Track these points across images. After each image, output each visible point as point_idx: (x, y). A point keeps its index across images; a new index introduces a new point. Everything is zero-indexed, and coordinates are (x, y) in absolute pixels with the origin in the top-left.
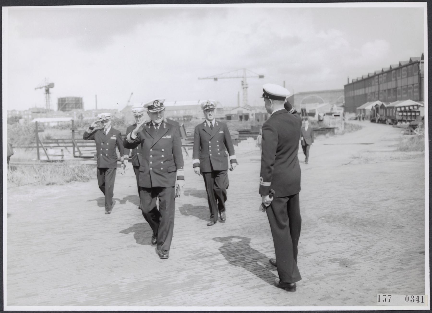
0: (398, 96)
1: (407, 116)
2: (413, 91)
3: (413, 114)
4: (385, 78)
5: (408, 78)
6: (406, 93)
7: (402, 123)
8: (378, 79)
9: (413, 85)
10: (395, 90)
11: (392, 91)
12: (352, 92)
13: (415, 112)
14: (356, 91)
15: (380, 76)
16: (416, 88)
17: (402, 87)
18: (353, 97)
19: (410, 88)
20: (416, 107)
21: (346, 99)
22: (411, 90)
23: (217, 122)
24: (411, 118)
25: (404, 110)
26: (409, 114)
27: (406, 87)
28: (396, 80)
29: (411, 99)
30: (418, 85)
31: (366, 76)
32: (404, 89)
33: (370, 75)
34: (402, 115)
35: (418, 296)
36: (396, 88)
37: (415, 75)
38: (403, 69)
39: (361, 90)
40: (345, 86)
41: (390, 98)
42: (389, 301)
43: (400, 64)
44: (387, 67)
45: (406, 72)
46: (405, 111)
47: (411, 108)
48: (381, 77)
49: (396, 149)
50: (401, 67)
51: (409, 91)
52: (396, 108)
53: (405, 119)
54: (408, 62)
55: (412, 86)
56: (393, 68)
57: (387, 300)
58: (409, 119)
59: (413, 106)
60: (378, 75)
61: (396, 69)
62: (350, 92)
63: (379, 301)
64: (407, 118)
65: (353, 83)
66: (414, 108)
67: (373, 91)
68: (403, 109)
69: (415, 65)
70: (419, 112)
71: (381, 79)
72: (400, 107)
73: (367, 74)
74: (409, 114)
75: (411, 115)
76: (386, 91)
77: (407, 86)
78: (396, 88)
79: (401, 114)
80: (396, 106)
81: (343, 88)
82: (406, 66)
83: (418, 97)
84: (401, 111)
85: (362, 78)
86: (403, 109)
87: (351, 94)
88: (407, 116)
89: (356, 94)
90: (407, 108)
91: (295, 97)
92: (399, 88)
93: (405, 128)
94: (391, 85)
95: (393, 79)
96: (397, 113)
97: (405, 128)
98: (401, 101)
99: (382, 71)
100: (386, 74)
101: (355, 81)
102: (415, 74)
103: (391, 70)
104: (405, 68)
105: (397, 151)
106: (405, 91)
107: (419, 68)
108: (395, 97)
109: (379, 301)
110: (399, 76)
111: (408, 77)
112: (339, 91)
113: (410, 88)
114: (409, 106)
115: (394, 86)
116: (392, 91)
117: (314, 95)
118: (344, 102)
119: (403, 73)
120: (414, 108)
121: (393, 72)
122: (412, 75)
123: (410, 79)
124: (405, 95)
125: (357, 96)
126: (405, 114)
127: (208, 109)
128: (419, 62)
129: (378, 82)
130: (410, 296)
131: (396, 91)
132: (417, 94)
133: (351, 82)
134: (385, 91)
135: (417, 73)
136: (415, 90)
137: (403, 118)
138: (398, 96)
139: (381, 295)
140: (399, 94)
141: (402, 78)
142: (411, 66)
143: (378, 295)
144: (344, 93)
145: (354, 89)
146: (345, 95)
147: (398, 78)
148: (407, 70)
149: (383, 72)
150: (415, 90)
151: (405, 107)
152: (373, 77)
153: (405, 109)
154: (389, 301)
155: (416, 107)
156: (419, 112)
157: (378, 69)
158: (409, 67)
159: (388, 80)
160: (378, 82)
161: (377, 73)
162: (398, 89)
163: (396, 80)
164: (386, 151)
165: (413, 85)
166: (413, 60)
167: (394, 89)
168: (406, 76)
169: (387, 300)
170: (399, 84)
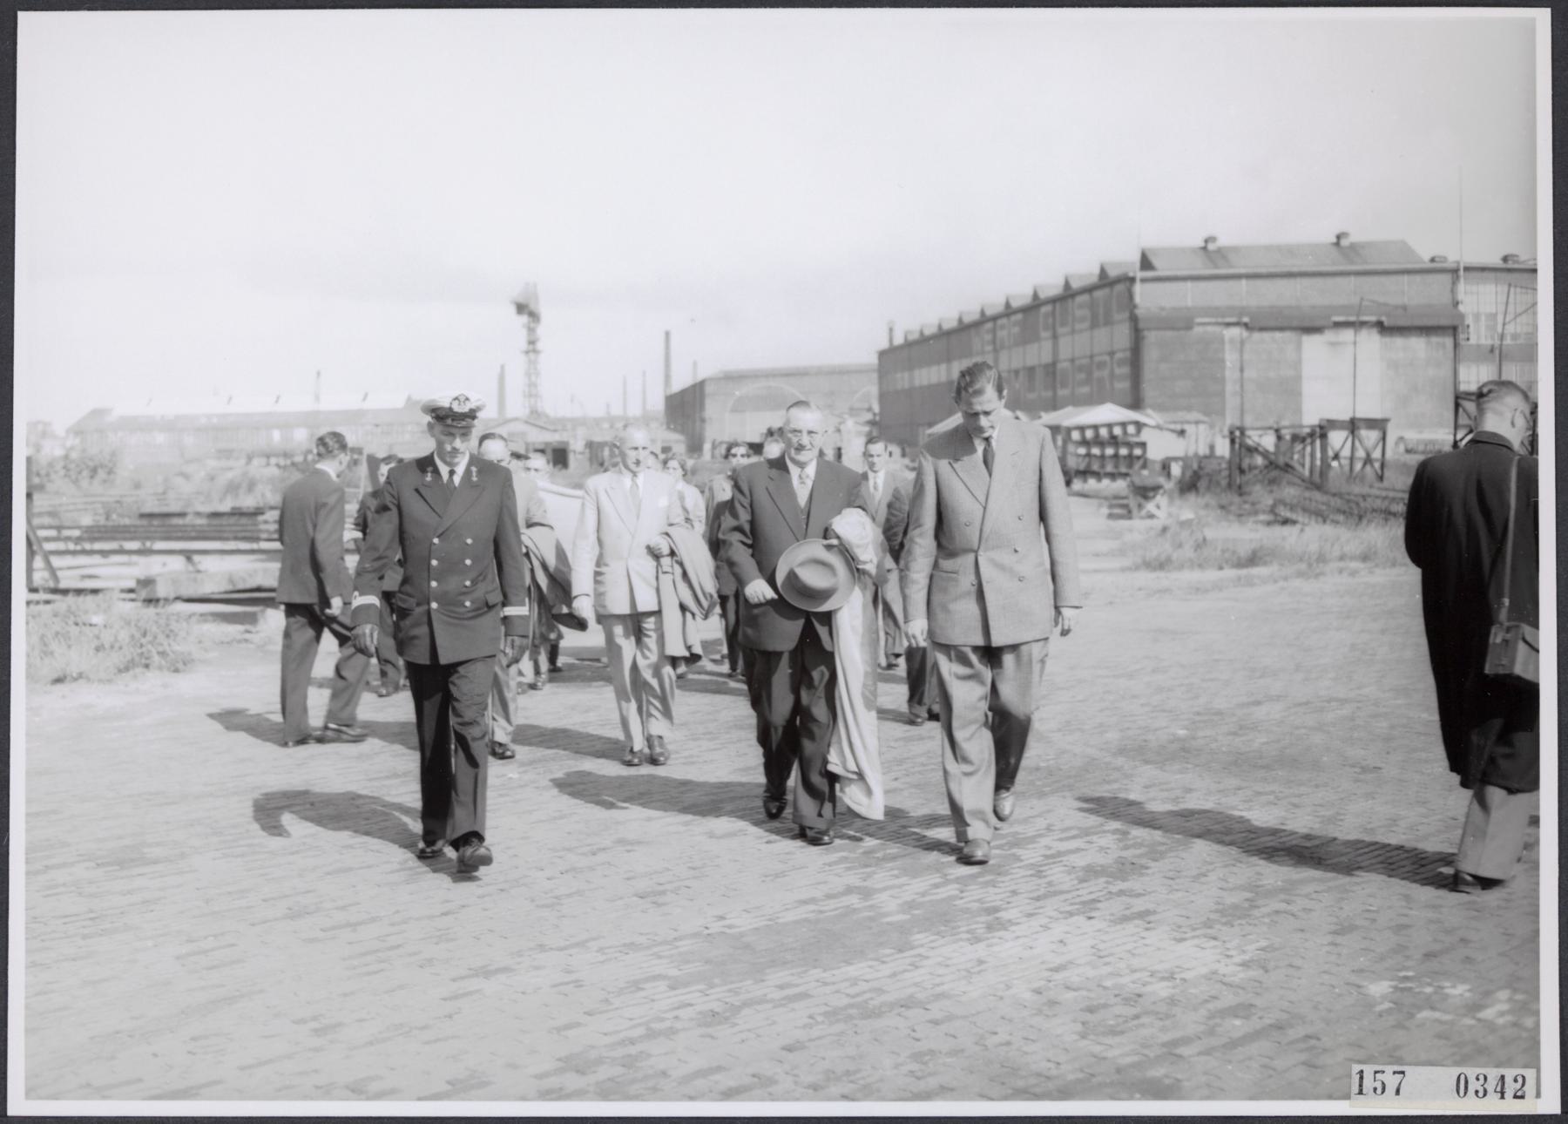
0: (1062, 392)
1: (1103, 457)
2: (1112, 376)
3: (1124, 451)
4: (1016, 330)
5: (1097, 332)
6: (1088, 381)
7: (1085, 481)
8: (994, 331)
9: (1111, 354)
10: (1051, 369)
11: (1039, 374)
12: (906, 375)
13: (1130, 445)
14: (917, 373)
15: (1000, 322)
16: (1121, 363)
17: (1072, 360)
18: (910, 393)
19: (1101, 365)
20: (1131, 429)
21: (882, 397)
22: (1105, 373)
23: (474, 469)
24: (1116, 466)
25: (1095, 438)
26: (1110, 451)
27: (1085, 361)
28: (1055, 337)
29: (1114, 402)
30: (1128, 354)
31: (951, 324)
32: (1080, 369)
33: (967, 319)
34: (1088, 455)
35: (1503, 1077)
36: (1054, 364)
37: (1081, 331)
38: (1080, 299)
39: (934, 369)
40: (882, 354)
41: (1032, 396)
42: (1398, 1092)
43: (1067, 285)
44: (1021, 293)
45: (1086, 312)
46: (1098, 441)
47: (1117, 431)
48: (1002, 327)
49: (1127, 562)
50: (1068, 294)
51: (1096, 374)
52: (1069, 430)
53: (1095, 467)
54: (1094, 279)
55: (1107, 358)
56: (1042, 295)
57: (1391, 1089)
58: (1109, 468)
59: (1124, 425)
60: (995, 318)
61: (1054, 301)
62: (899, 375)
63: (1361, 1093)
64: (1103, 466)
65: (909, 344)
66: (1125, 432)
67: (1031, 361)
68: (1089, 434)
69: (1120, 288)
70: (1143, 445)
71: (1002, 334)
72: (1082, 429)
73: (936, 322)
74: (1110, 451)
75: (1116, 456)
76: (1021, 374)
77: (1091, 357)
78: (1054, 364)
79: (1082, 451)
80: (1067, 423)
81: (873, 360)
82: (1089, 290)
83: (1435, 339)
84: (1084, 442)
85: (940, 327)
86: (1089, 434)
87: (902, 380)
88: (1103, 457)
89: (917, 383)
90: (1104, 432)
91: (709, 389)
92: (1063, 365)
93: (1106, 498)
94: (1038, 353)
95: (1045, 334)
96: (1071, 448)
97: (1106, 498)
98: (1081, 409)
99: (1008, 305)
100: (1019, 316)
101: (916, 336)
102: (1117, 317)
103: (1036, 303)
104: (1085, 298)
105: (1137, 568)
106: (1082, 376)
107: (1131, 296)
108: (1049, 394)
109: (1361, 1093)
110: (1063, 324)
111: (1094, 325)
112: (860, 371)
113: (1101, 365)
114: (1110, 426)
115: (1047, 358)
116: (1039, 374)
117: (773, 383)
118: (876, 409)
119: (1079, 313)
120: (1125, 432)
121: (1044, 309)
122: (1108, 322)
123: (1102, 334)
124: (1085, 390)
125: (921, 387)
126: (1096, 451)
127: (449, 421)
128: (1132, 280)
129: (994, 342)
130: (1510, 1074)
131: (1054, 373)
132: (1123, 385)
133: (899, 340)
134: (1017, 372)
135: (1126, 315)
136: (1118, 371)
137: (1089, 464)
138: (1062, 392)
139: (1368, 1070)
140: (1064, 385)
141: (1073, 332)
142: (1106, 291)
143: (1356, 1068)
144: (875, 376)
145: (911, 366)
146: (880, 383)
147: (1060, 330)
148: (1092, 306)
149: (1009, 311)
150: (1118, 371)
151: (1096, 427)
152: (976, 325)
153: (1097, 435)
154: (1398, 1092)
155: (1131, 429)
156: (1143, 445)
157: (994, 300)
158: (1098, 294)
159: (1028, 336)
160: (994, 342)
161: (989, 313)
162: (1060, 366)
163: (1055, 337)
164: (1096, 571)
165: (1111, 354)
166: (1113, 273)
167: (1046, 366)
168: (1086, 324)
169: (1391, 1089)
170: (1065, 351)
